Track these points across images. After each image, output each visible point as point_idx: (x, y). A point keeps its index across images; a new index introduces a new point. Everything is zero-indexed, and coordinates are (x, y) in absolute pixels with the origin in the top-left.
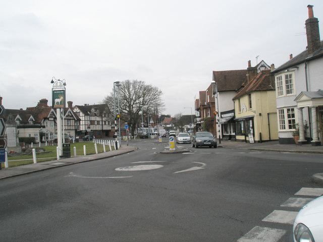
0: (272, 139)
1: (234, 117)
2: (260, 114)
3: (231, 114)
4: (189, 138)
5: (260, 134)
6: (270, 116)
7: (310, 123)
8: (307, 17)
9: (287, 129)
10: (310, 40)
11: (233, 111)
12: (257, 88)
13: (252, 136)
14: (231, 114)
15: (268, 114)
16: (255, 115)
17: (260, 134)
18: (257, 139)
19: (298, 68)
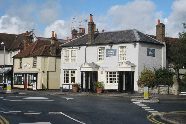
0: (49, 88)
1: (12, 70)
2: (43, 72)
3: (11, 68)
4: (174, 89)
5: (42, 84)
6: (50, 73)
7: (180, 116)
8: (89, 21)
9: (70, 83)
10: (90, 32)
11: (12, 66)
12: (43, 54)
13: (36, 86)
14: (11, 68)
15: (48, 72)
16: (39, 71)
17: (42, 84)
18: (39, 87)
19: (80, 48)
